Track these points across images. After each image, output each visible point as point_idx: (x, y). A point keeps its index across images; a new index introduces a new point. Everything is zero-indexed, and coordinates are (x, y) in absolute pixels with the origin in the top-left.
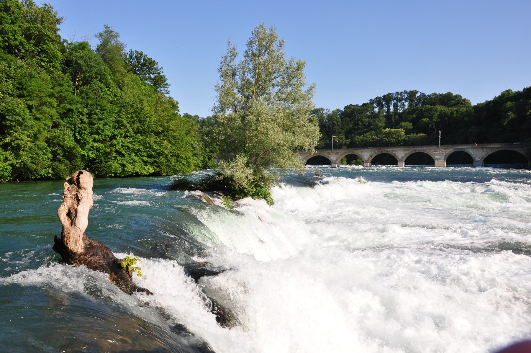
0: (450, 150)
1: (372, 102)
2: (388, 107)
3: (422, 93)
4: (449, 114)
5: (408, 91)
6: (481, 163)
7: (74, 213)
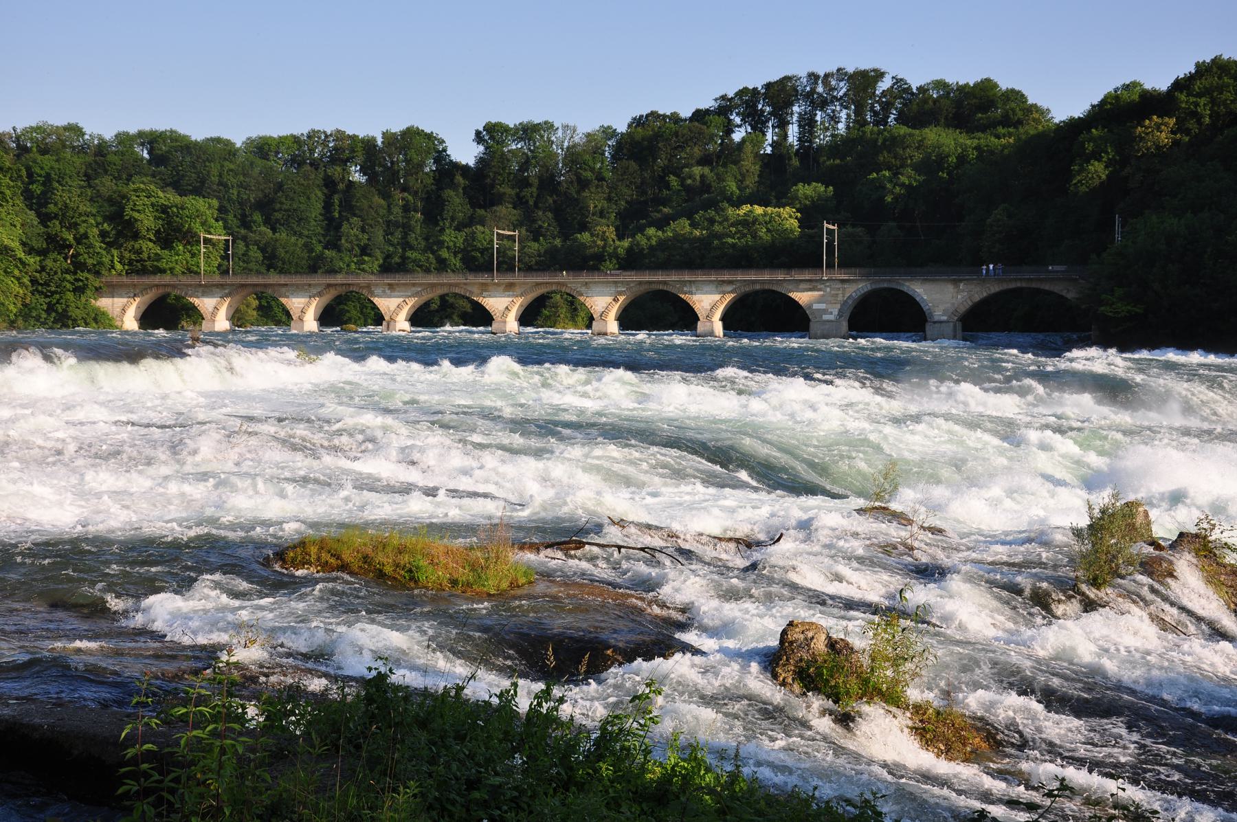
0: (856, 287)
1: (725, 106)
2: (783, 125)
3: (898, 81)
4: (953, 159)
5: (850, 69)
6: (949, 329)
7: (1034, 548)
